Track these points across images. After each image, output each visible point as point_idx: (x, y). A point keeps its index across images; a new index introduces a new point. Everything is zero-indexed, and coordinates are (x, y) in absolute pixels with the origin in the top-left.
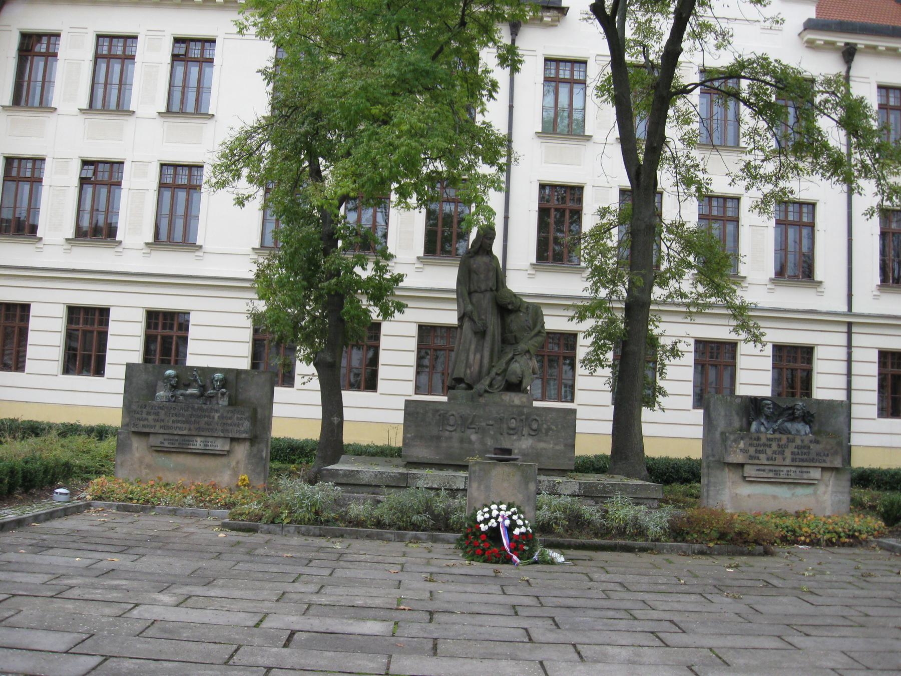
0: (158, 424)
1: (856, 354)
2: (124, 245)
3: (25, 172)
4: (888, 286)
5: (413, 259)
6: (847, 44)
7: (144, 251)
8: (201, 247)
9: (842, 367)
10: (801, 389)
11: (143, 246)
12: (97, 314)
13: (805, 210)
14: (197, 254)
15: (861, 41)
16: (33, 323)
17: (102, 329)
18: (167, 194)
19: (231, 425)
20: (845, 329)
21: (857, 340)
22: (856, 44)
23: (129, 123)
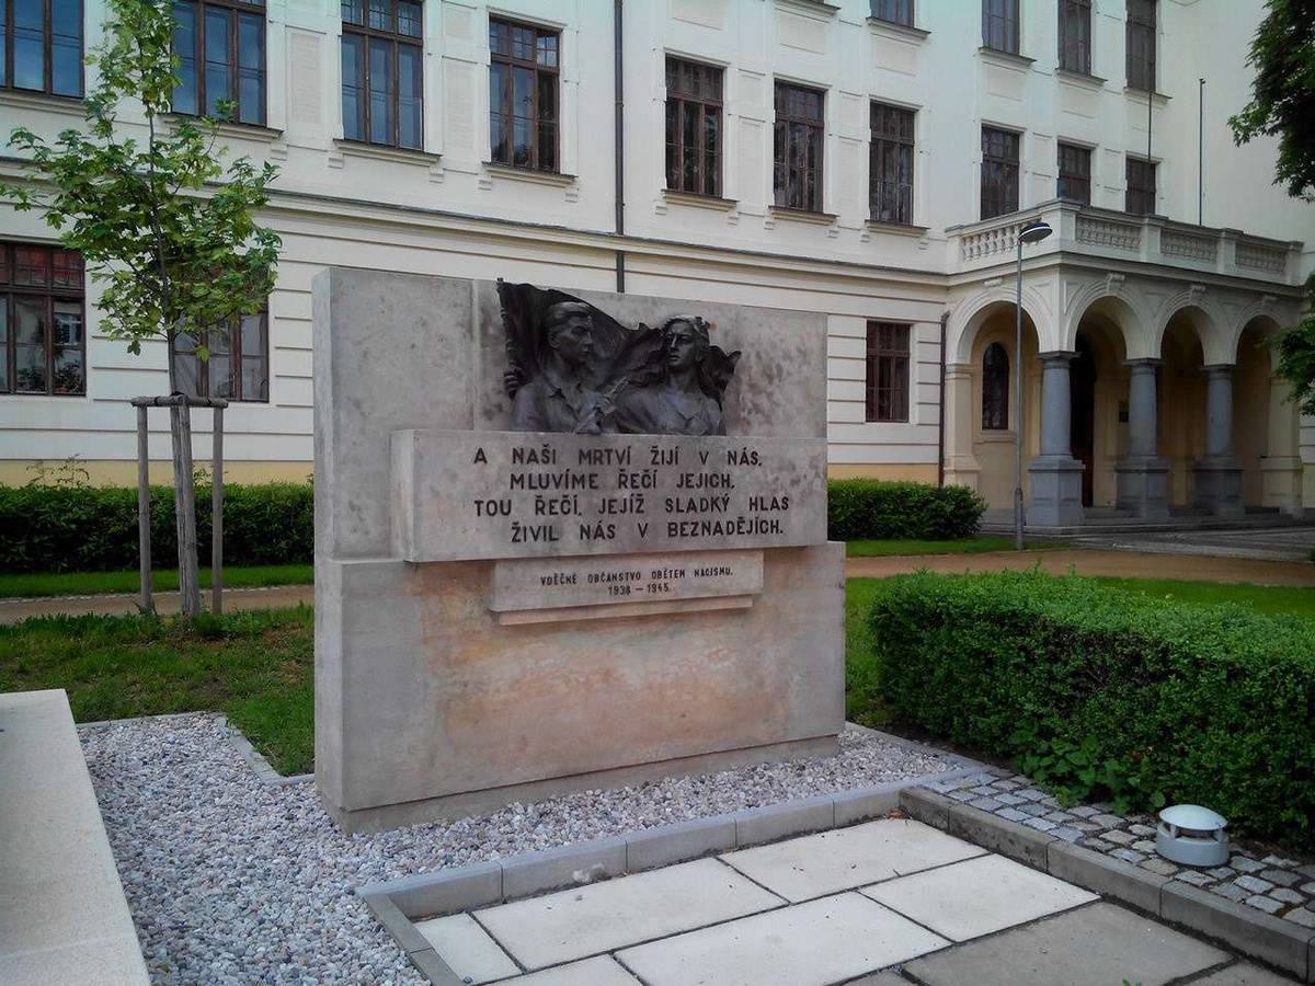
20: (613, 264)
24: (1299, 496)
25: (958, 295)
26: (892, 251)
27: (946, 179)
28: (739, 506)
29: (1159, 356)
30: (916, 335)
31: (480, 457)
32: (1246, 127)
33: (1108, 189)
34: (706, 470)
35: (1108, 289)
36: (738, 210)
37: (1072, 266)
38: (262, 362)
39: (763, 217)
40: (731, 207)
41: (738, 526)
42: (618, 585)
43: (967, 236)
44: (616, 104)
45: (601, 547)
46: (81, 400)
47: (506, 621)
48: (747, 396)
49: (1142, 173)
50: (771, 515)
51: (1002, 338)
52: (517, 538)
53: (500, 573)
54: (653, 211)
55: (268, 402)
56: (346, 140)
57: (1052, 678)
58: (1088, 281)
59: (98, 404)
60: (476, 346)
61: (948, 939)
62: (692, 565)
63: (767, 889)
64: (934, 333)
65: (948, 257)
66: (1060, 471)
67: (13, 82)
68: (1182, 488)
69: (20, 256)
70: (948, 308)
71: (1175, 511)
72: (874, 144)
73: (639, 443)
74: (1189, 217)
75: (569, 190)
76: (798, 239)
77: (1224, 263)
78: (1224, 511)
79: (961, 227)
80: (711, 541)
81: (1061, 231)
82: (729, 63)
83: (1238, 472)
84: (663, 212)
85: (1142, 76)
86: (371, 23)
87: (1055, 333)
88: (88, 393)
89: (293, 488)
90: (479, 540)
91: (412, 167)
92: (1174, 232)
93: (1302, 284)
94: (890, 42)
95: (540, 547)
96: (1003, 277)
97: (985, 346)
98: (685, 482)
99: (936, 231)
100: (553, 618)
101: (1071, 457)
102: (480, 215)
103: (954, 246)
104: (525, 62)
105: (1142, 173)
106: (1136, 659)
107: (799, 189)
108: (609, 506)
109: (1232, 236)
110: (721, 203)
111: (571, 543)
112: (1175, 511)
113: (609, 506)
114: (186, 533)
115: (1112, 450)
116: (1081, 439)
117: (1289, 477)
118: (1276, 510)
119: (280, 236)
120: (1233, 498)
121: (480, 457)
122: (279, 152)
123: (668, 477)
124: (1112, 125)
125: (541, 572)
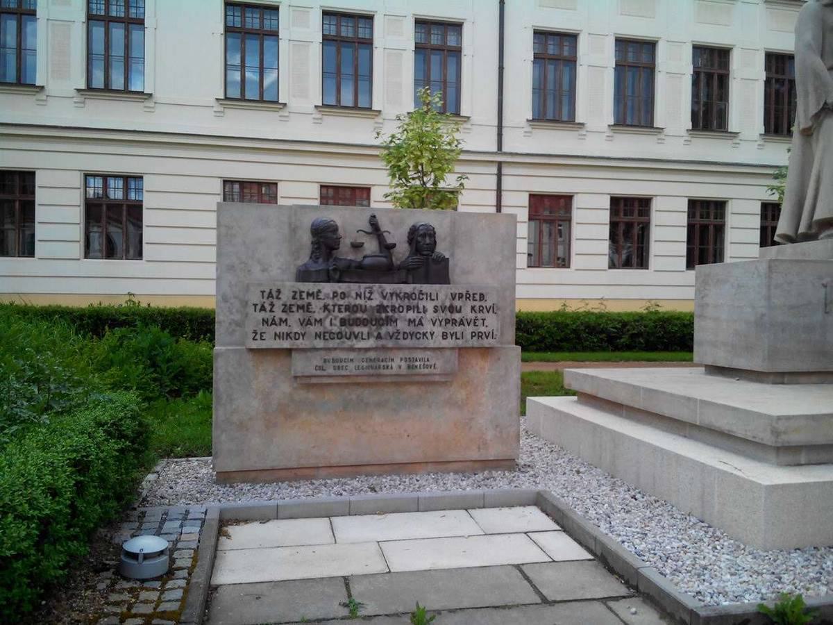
0: (313, 329)
2: (384, 115)
4: (699, 130)
7: (75, 100)
8: (42, 88)
10: (708, 249)
11: (74, 93)
12: (636, 204)
14: (281, 113)
16: (41, 196)
17: (643, 219)
18: (99, 32)
19: (462, 323)
20: (494, 170)
21: (507, 183)
36: (472, 122)
38: (565, 249)
39: (756, 141)
40: (660, 132)
44: (499, 68)
46: (647, 271)
52: (399, 337)
55: (569, 267)
56: (533, 120)
59: (656, 273)
61: (610, 609)
67: (244, 96)
69: (341, 191)
72: (768, 82)
82: (465, 19)
84: (610, 138)
86: (448, 42)
88: (36, 255)
89: (637, 314)
91: (127, 103)
102: (637, 157)
104: (348, 39)
109: (347, 70)
110: (372, 113)
114: (285, 337)
119: (468, 175)
122: (582, 135)
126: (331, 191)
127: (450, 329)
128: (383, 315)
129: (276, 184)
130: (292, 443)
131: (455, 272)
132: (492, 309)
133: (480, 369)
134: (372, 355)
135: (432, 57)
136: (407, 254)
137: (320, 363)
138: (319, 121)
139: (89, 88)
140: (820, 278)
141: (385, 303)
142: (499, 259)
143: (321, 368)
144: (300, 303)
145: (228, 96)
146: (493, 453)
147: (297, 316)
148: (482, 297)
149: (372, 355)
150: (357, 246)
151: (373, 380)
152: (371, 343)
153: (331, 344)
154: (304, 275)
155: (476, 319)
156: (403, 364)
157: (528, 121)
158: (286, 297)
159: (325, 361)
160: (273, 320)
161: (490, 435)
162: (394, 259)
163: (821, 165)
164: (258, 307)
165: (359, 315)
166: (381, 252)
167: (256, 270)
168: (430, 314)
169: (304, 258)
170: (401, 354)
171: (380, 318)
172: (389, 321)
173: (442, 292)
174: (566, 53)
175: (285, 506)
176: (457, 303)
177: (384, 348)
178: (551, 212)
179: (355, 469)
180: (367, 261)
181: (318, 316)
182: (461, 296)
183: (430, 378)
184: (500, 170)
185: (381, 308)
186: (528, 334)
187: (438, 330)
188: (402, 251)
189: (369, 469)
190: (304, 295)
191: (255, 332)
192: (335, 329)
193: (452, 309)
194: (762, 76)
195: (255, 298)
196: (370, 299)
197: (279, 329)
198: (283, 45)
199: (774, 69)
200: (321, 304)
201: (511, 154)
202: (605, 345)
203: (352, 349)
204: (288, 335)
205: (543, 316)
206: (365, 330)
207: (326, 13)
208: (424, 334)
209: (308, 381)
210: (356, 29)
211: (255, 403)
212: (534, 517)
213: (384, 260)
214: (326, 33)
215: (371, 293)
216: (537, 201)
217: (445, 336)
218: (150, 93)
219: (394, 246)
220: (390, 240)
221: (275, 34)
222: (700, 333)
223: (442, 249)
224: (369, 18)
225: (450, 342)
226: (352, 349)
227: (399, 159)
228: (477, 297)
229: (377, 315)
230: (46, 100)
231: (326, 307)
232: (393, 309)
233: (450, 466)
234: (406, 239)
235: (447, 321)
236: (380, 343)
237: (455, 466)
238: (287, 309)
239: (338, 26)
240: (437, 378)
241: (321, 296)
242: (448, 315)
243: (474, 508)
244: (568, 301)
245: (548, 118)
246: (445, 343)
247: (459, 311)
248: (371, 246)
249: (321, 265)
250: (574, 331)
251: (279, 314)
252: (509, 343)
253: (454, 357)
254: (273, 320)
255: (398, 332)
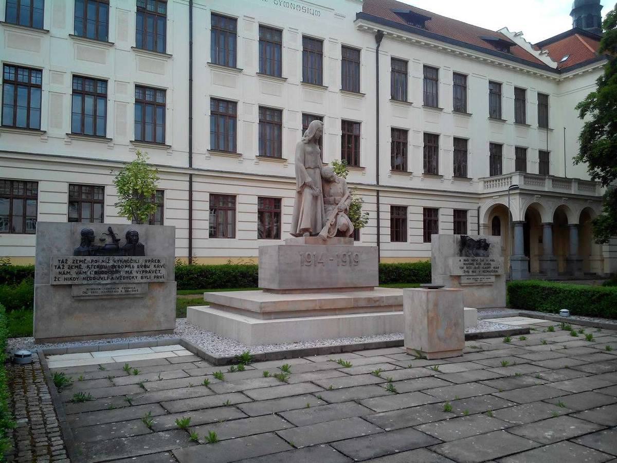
0: (82, 276)
1: (196, 196)
3: (24, 80)
5: (63, 135)
6: (379, 31)
9: (186, 205)
13: (230, 106)
14: (240, 159)
15: (386, 30)
19: (150, 272)
22: (383, 31)
23: (45, 40)
24: (603, 269)
25: (484, 200)
26: (461, 186)
27: (478, 162)
28: (492, 269)
29: (552, 222)
30: (469, 214)
31: (460, 261)
32: (577, 160)
33: (533, 167)
34: (487, 262)
35: (534, 200)
37: (524, 193)
41: (492, 271)
42: (476, 280)
43: (486, 181)
45: (474, 274)
47: (463, 285)
48: (490, 251)
49: (544, 157)
50: (496, 270)
51: (499, 216)
53: (462, 277)
54: (388, 178)
57: (542, 295)
58: (528, 198)
60: (455, 244)
62: (486, 277)
63: (445, 380)
64: (475, 213)
65: (479, 188)
66: (521, 260)
68: (562, 266)
70: (480, 204)
71: (559, 274)
73: (478, 258)
74: (562, 175)
75: (364, 172)
76: (431, 184)
77: (574, 190)
78: (577, 274)
79: (484, 178)
80: (488, 274)
81: (517, 180)
83: (581, 261)
85: (544, 122)
87: (517, 213)
90: (460, 273)
92: (556, 180)
93: (602, 195)
94: (460, 118)
95: (467, 274)
96: (499, 196)
97: (492, 218)
98: (484, 264)
99: (475, 179)
100: (468, 284)
101: (524, 256)
103: (481, 184)
105: (544, 157)
106: (556, 291)
107: (431, 169)
108: (475, 268)
111: (471, 273)
112: (559, 274)
113: (475, 268)
115: (536, 252)
116: (527, 251)
117: (599, 263)
118: (595, 274)
120: (580, 269)
121: (460, 261)
123: (482, 263)
124: (534, 140)
125: (467, 277)
126: (76, 188)
127: (144, 274)
128: (114, 269)
129: (38, 182)
130: (71, 325)
131: (147, 250)
132: (163, 266)
133: (158, 292)
134: (109, 286)
135: (159, 21)
136: (126, 243)
137: (85, 290)
138: (70, 143)
139: (73, 133)
140: (299, 252)
141: (115, 264)
142: (167, 245)
143: (86, 293)
144: (76, 265)
145: (3, 124)
146: (164, 327)
147: (76, 270)
148: (159, 261)
149: (109, 286)
150: (102, 240)
151: (109, 297)
152: (109, 281)
153: (90, 282)
154: (77, 253)
155: (156, 270)
156: (123, 290)
157: (208, 150)
158: (70, 262)
159: (87, 289)
160: (64, 272)
161: (162, 319)
162: (119, 246)
163: (304, 206)
164: (57, 267)
165: (103, 270)
166: (113, 242)
167: (55, 252)
168: (136, 269)
169: (78, 245)
170: (122, 286)
171: (113, 270)
172: (117, 272)
173: (141, 259)
174: (230, 112)
175: (70, 348)
176: (148, 264)
177: (115, 283)
178: (222, 205)
179: (101, 336)
180: (107, 246)
181: (84, 270)
182: (149, 261)
183: (135, 296)
184: (191, 178)
185: (113, 266)
186: (207, 278)
187: (139, 275)
188: (123, 242)
189: (107, 336)
190: (78, 262)
191: (56, 278)
192: (92, 276)
193: (145, 266)
194: (340, 133)
195: (56, 263)
196: (108, 263)
197: (66, 276)
198: (45, 94)
199: (346, 129)
200: (86, 265)
201: (198, 170)
202: (252, 283)
203: (99, 284)
204: (70, 279)
205: (216, 267)
206: (106, 276)
207: (75, 77)
208: (133, 277)
209: (78, 298)
210: (95, 87)
211: (54, 309)
212: (179, 347)
213: (115, 246)
214: (75, 88)
215: (109, 260)
216: (214, 197)
217: (142, 278)
218: (45, 130)
219: (120, 240)
220: (118, 238)
221: (39, 87)
222: (262, 275)
223: (141, 241)
224: (105, 82)
225: (144, 280)
226: (99, 284)
227: (124, 185)
228: (157, 261)
229: (112, 269)
230: (113, 147)
231: (88, 266)
232: (119, 267)
233: (144, 333)
234: (125, 237)
235: (143, 271)
236: (113, 281)
237: (146, 333)
238: (70, 267)
239: (83, 85)
240: (139, 296)
241: (86, 262)
242: (144, 269)
243: (153, 346)
244: (232, 258)
245: (220, 149)
246: (142, 281)
247: (149, 267)
248: (109, 240)
249: (86, 248)
250: (234, 276)
251: (66, 269)
252: (173, 280)
253: (147, 286)
254: (64, 272)
255: (121, 276)
